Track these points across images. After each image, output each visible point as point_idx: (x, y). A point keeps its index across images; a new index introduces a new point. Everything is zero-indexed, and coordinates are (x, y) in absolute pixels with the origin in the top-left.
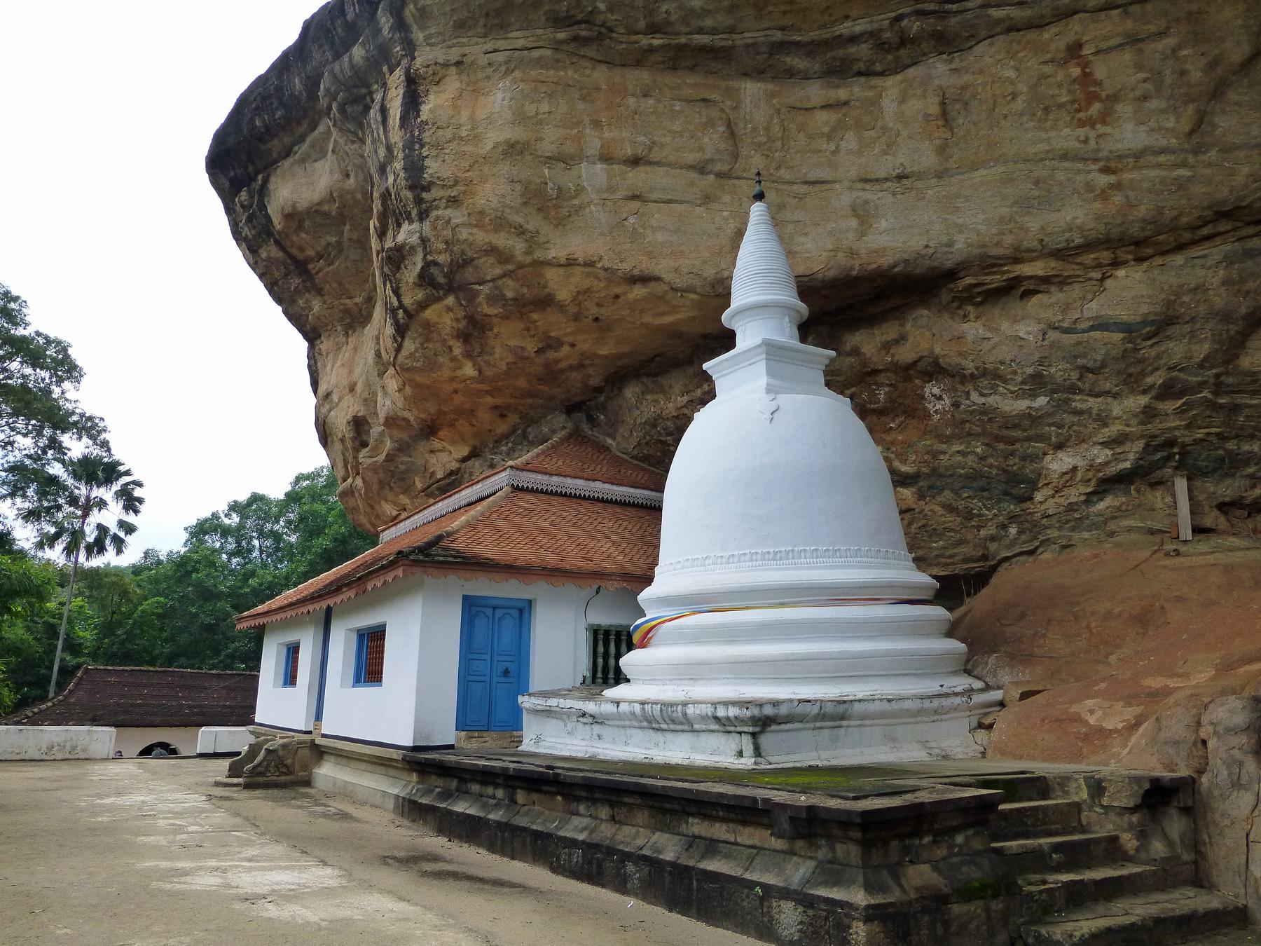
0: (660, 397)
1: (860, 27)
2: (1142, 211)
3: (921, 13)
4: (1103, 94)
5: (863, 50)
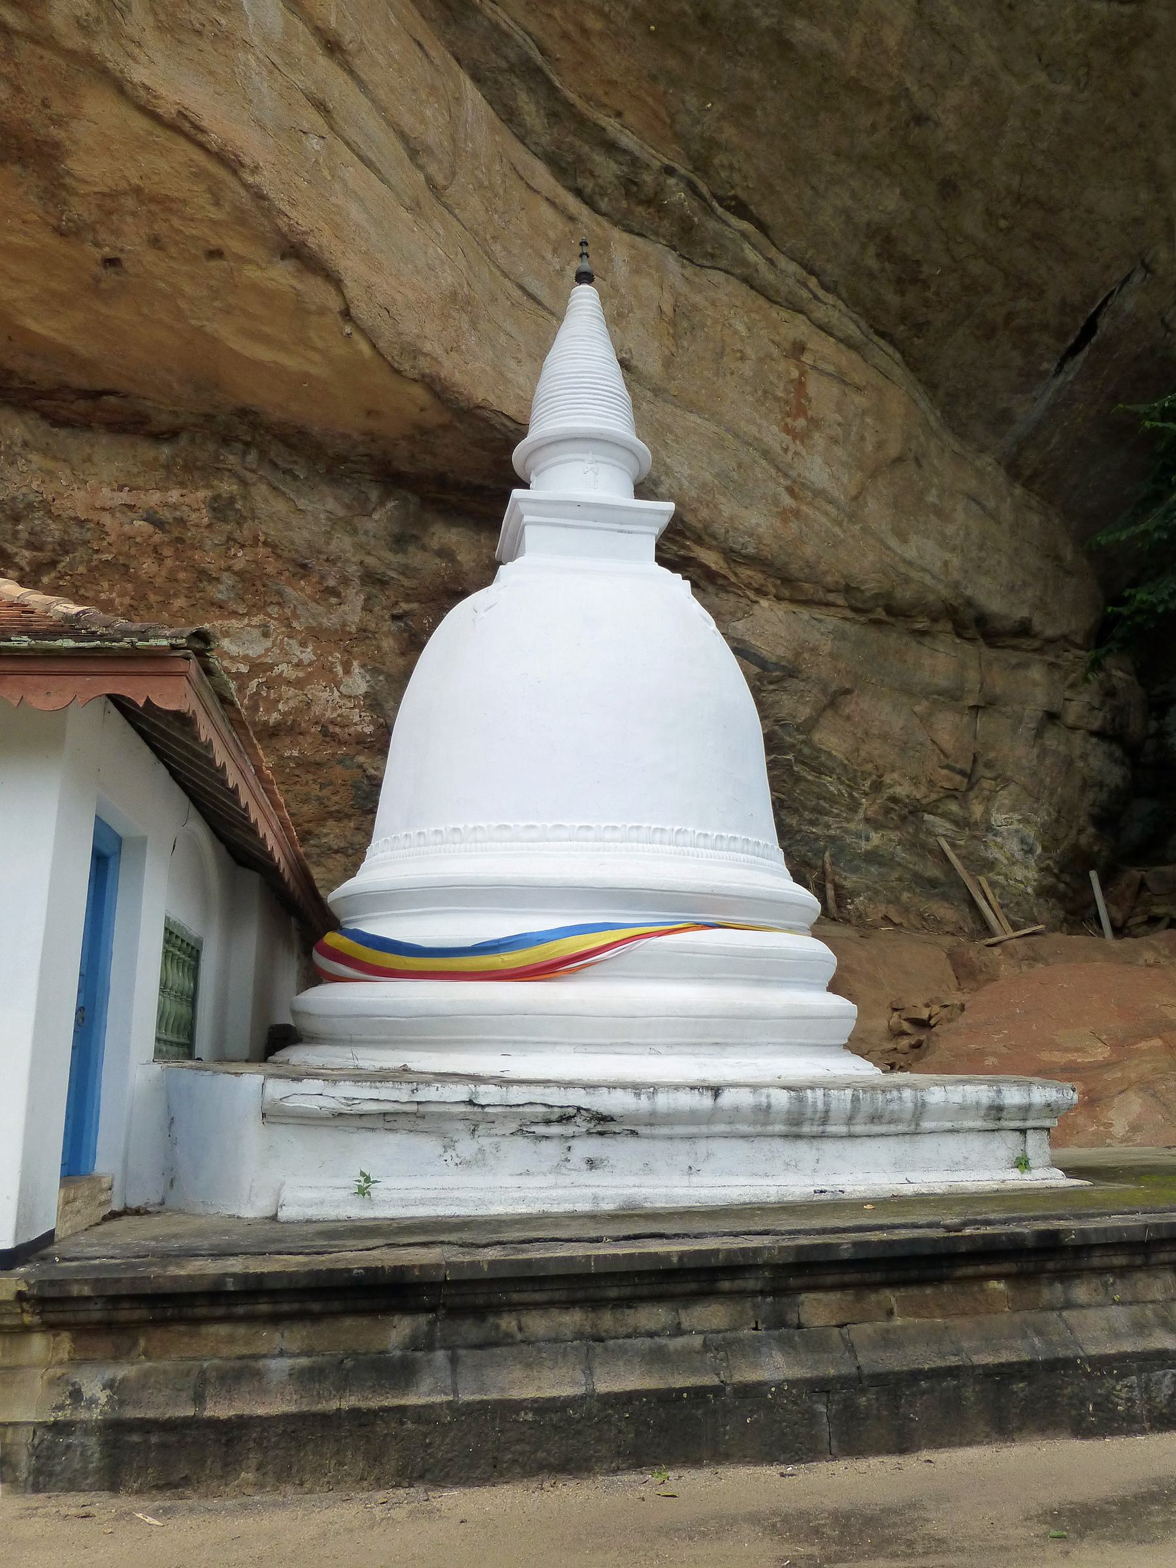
0: (64, 474)
1: (628, 140)
2: (809, 551)
3: (692, 188)
4: (810, 413)
5: (608, 169)
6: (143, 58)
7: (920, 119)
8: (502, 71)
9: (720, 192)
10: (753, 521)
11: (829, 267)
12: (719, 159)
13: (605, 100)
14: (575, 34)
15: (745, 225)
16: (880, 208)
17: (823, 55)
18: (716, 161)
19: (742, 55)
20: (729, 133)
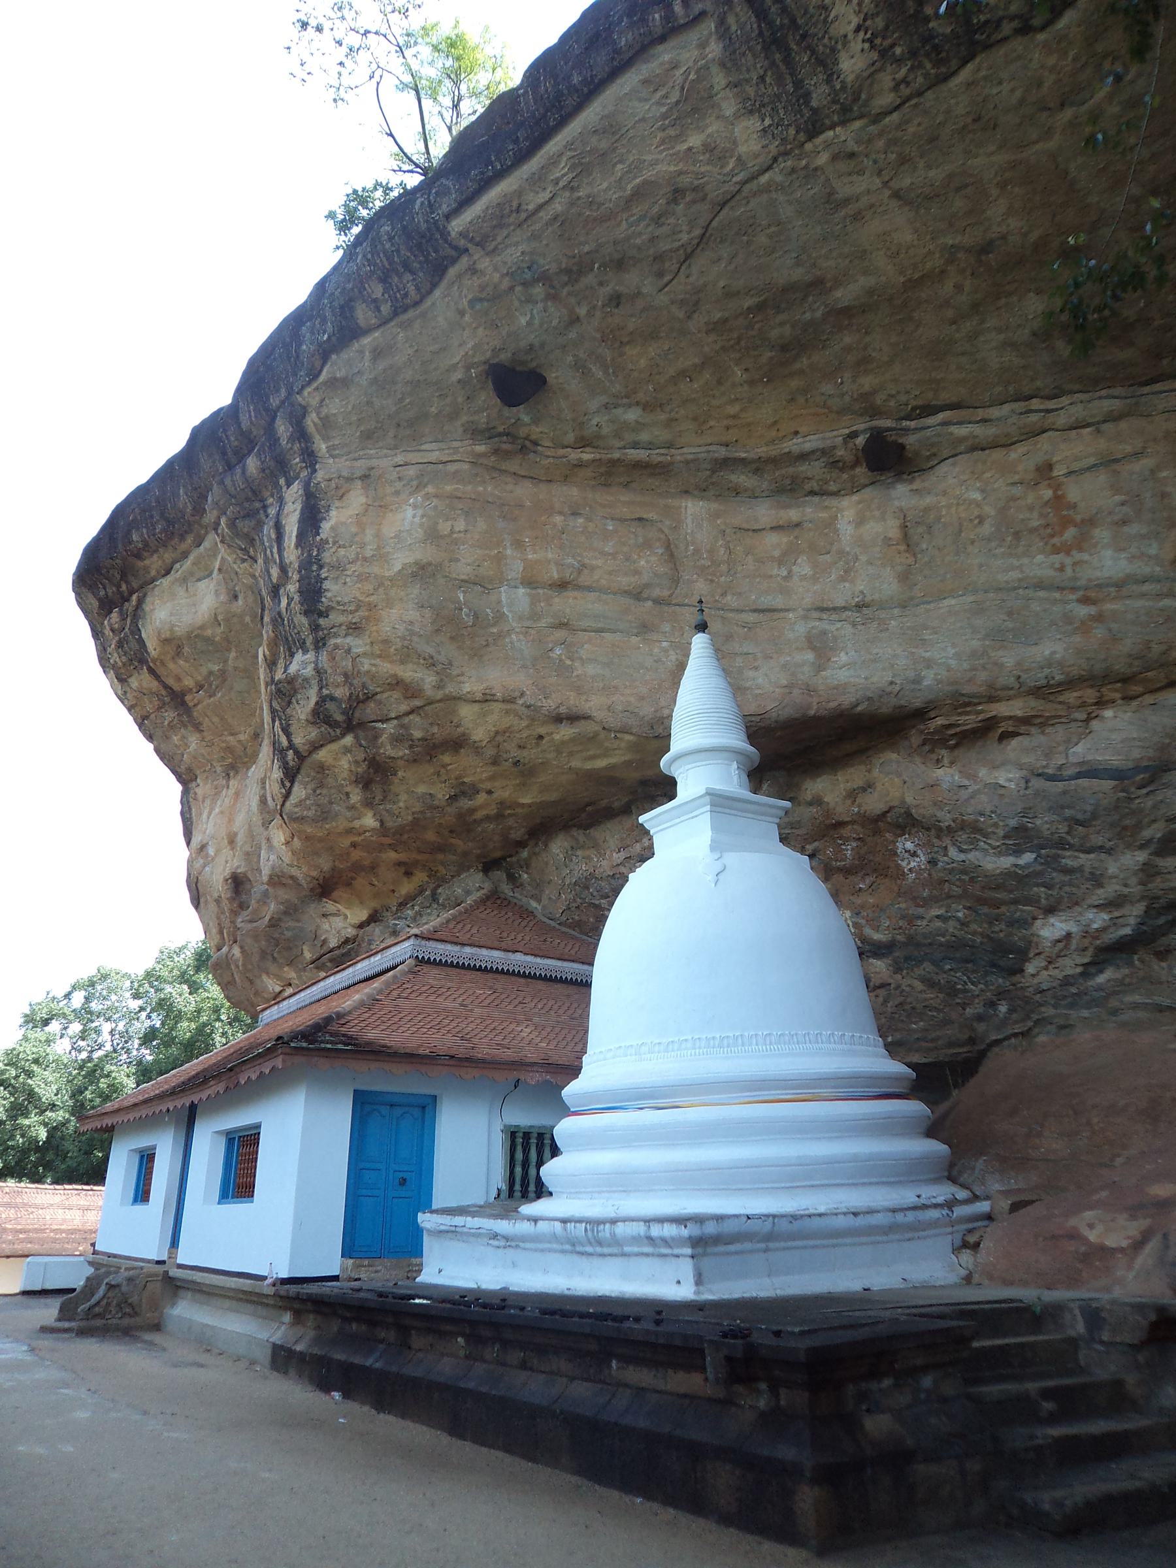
6: (466, 679)
7: (986, 248)
8: (710, 477)
9: (902, 414)
10: (1047, 653)
11: (1039, 383)
12: (879, 400)
13: (781, 434)
14: (730, 422)
15: (941, 416)
16: (1031, 317)
17: (871, 292)
18: (879, 402)
19: (828, 339)
20: (867, 382)
